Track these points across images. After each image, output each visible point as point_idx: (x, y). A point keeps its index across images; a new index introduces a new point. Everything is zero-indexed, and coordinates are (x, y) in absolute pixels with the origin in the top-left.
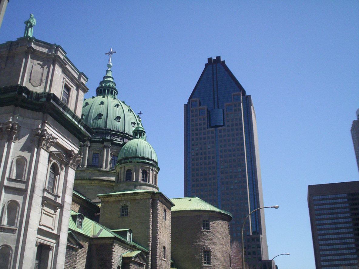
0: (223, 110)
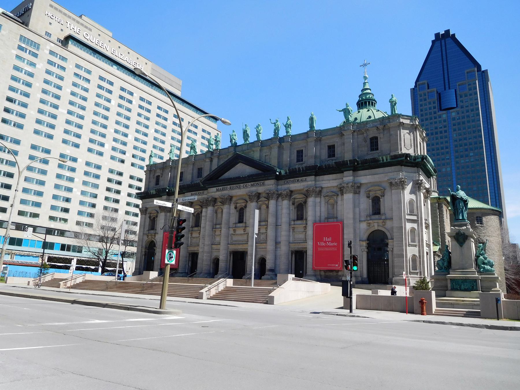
0: (455, 90)
